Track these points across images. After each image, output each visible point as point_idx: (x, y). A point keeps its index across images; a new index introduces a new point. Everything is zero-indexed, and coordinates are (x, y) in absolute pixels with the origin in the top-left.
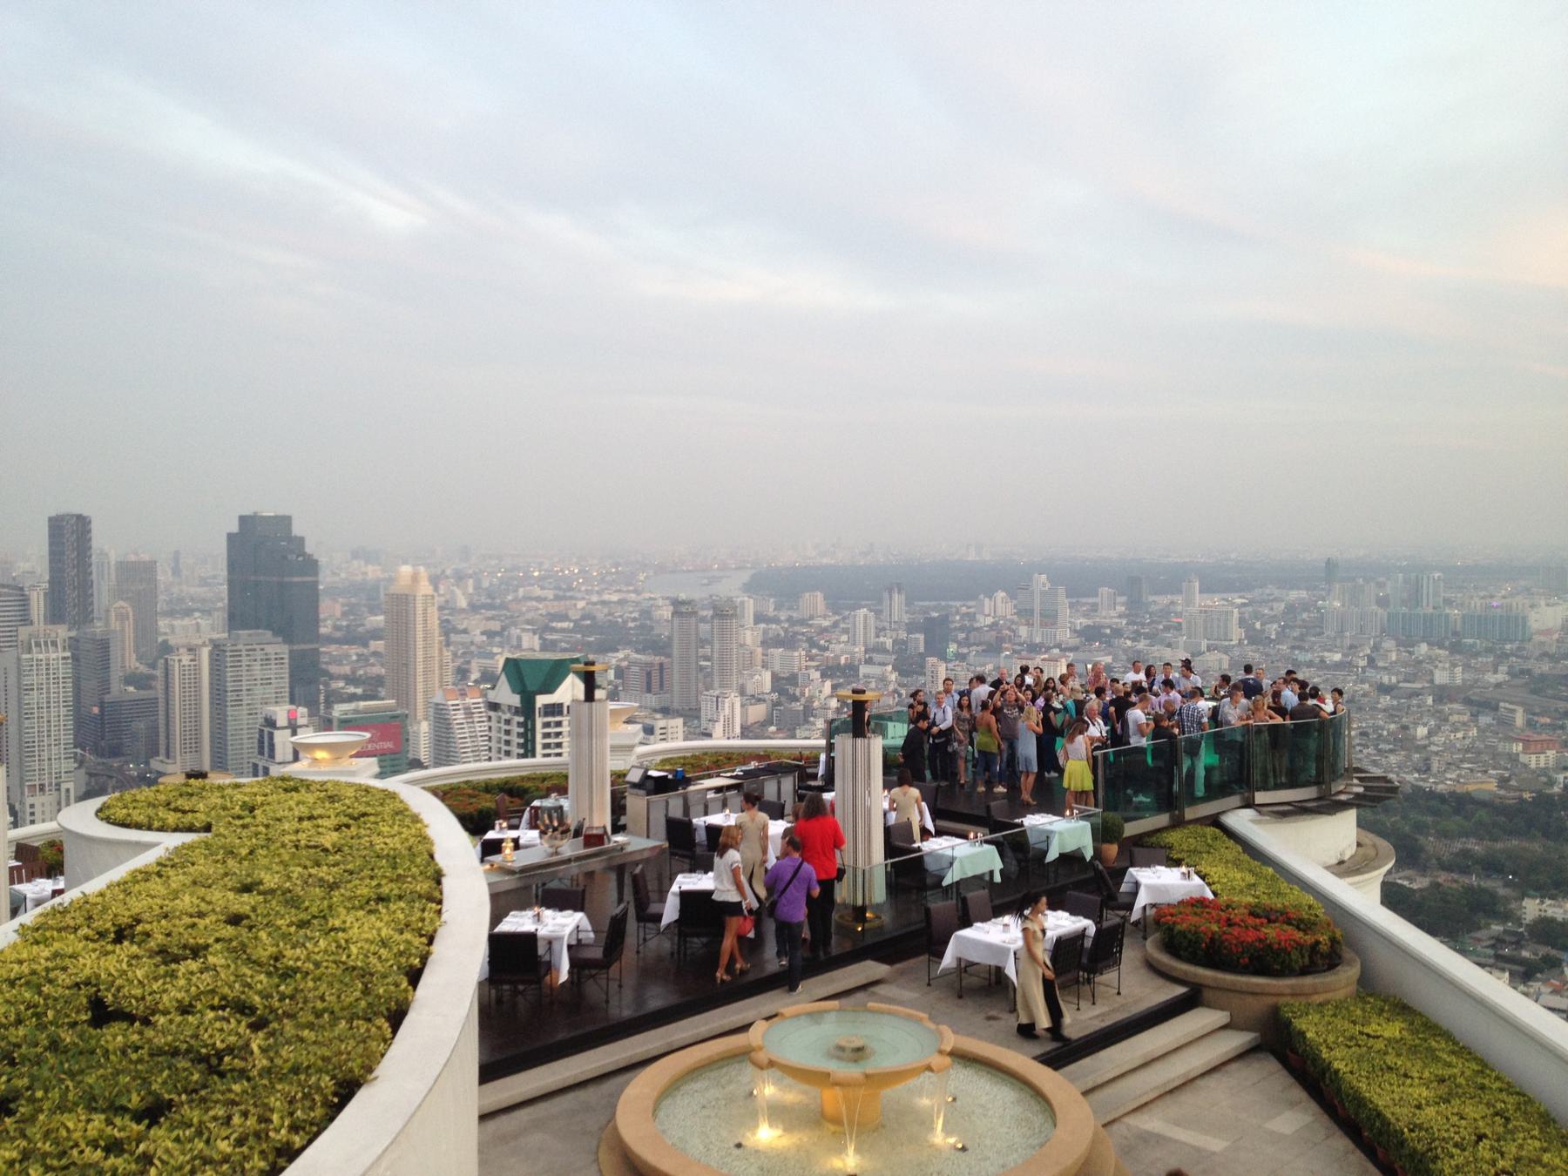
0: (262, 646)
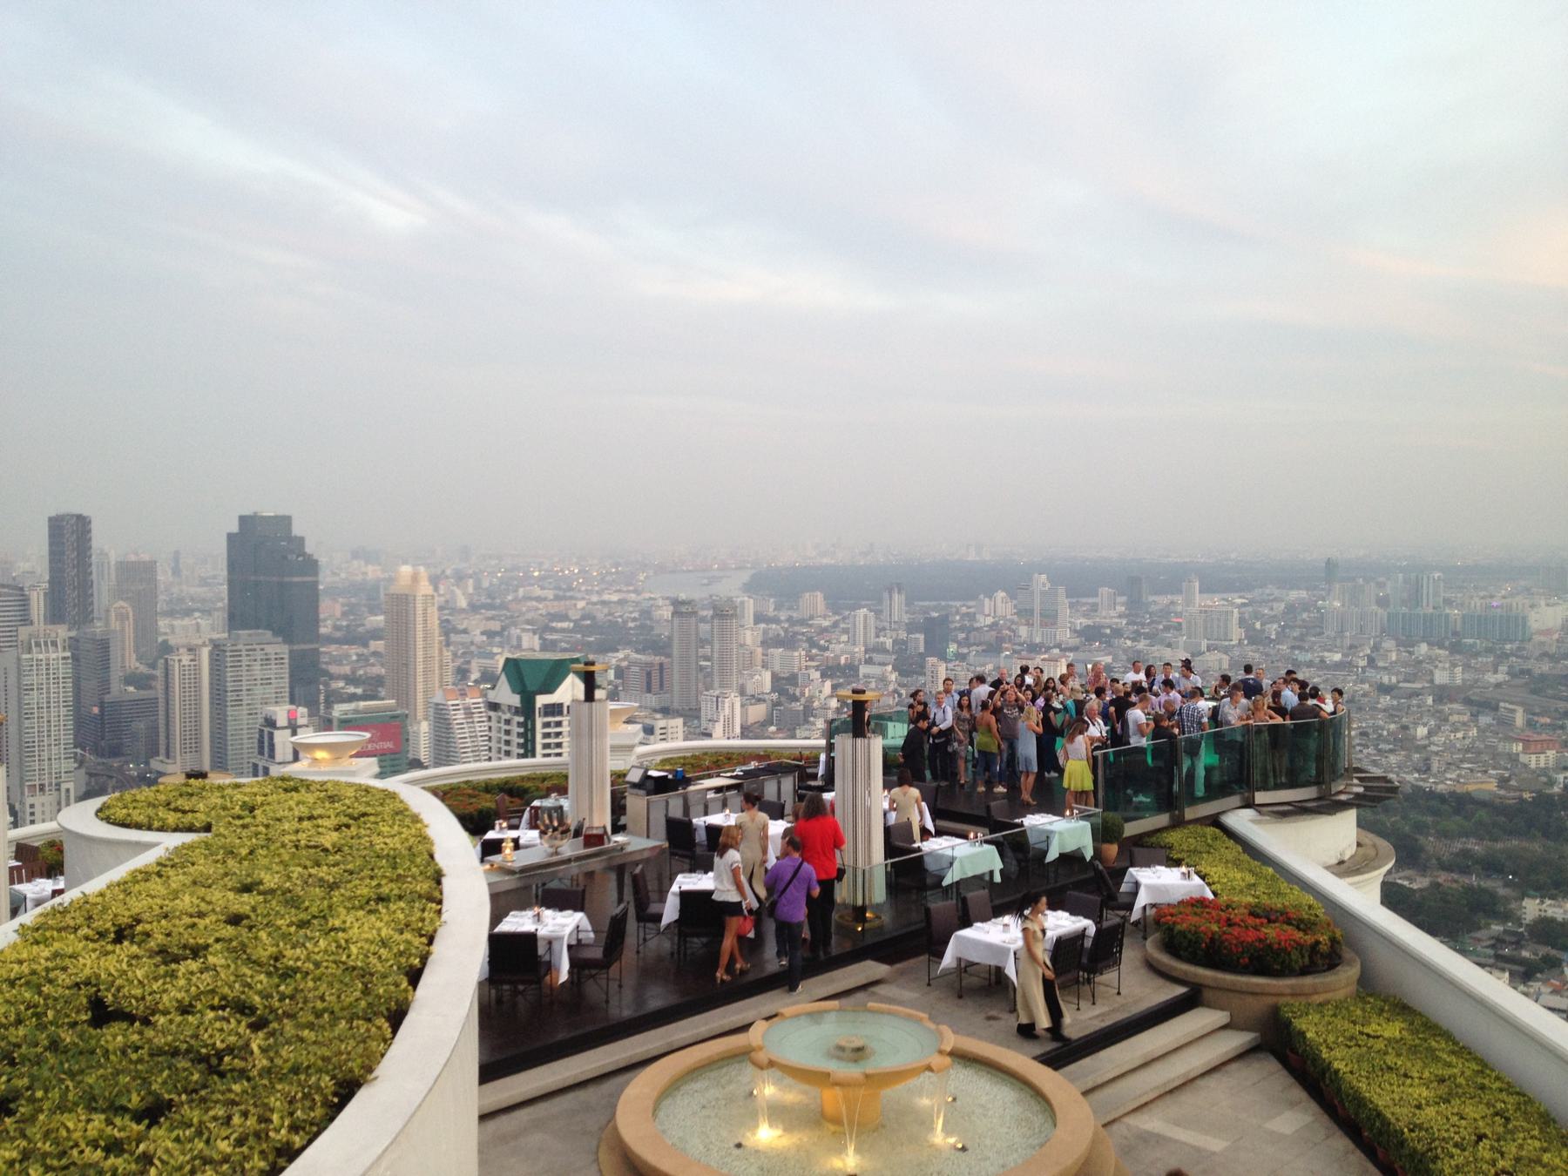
0: (262, 646)
